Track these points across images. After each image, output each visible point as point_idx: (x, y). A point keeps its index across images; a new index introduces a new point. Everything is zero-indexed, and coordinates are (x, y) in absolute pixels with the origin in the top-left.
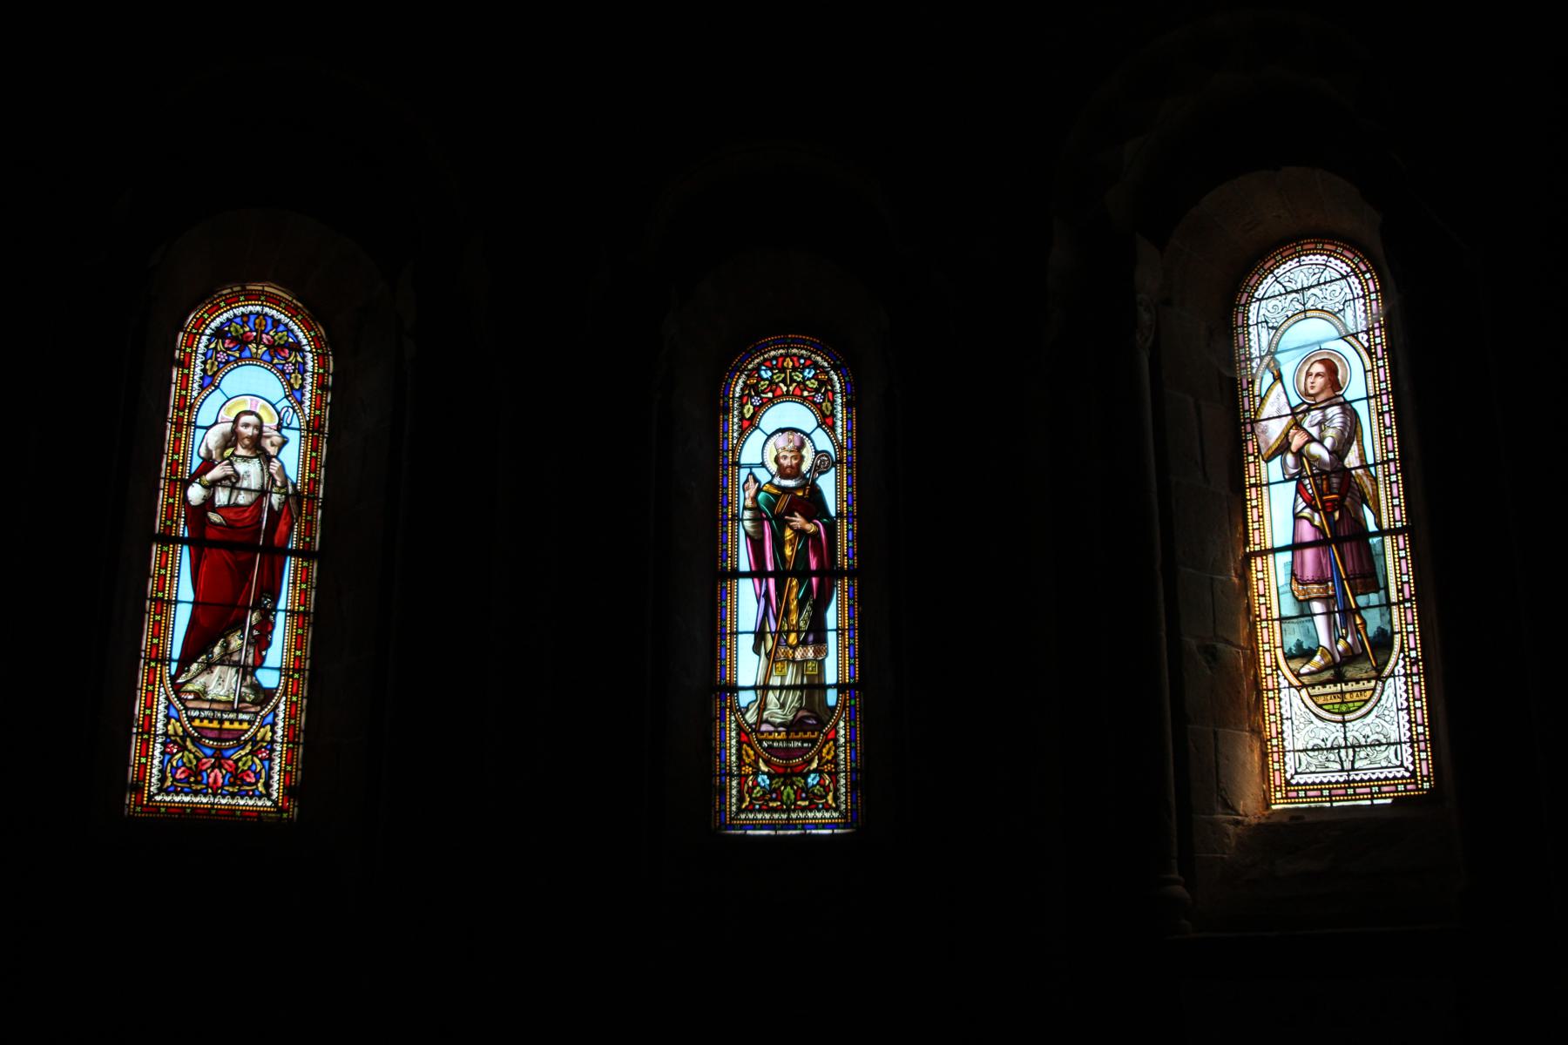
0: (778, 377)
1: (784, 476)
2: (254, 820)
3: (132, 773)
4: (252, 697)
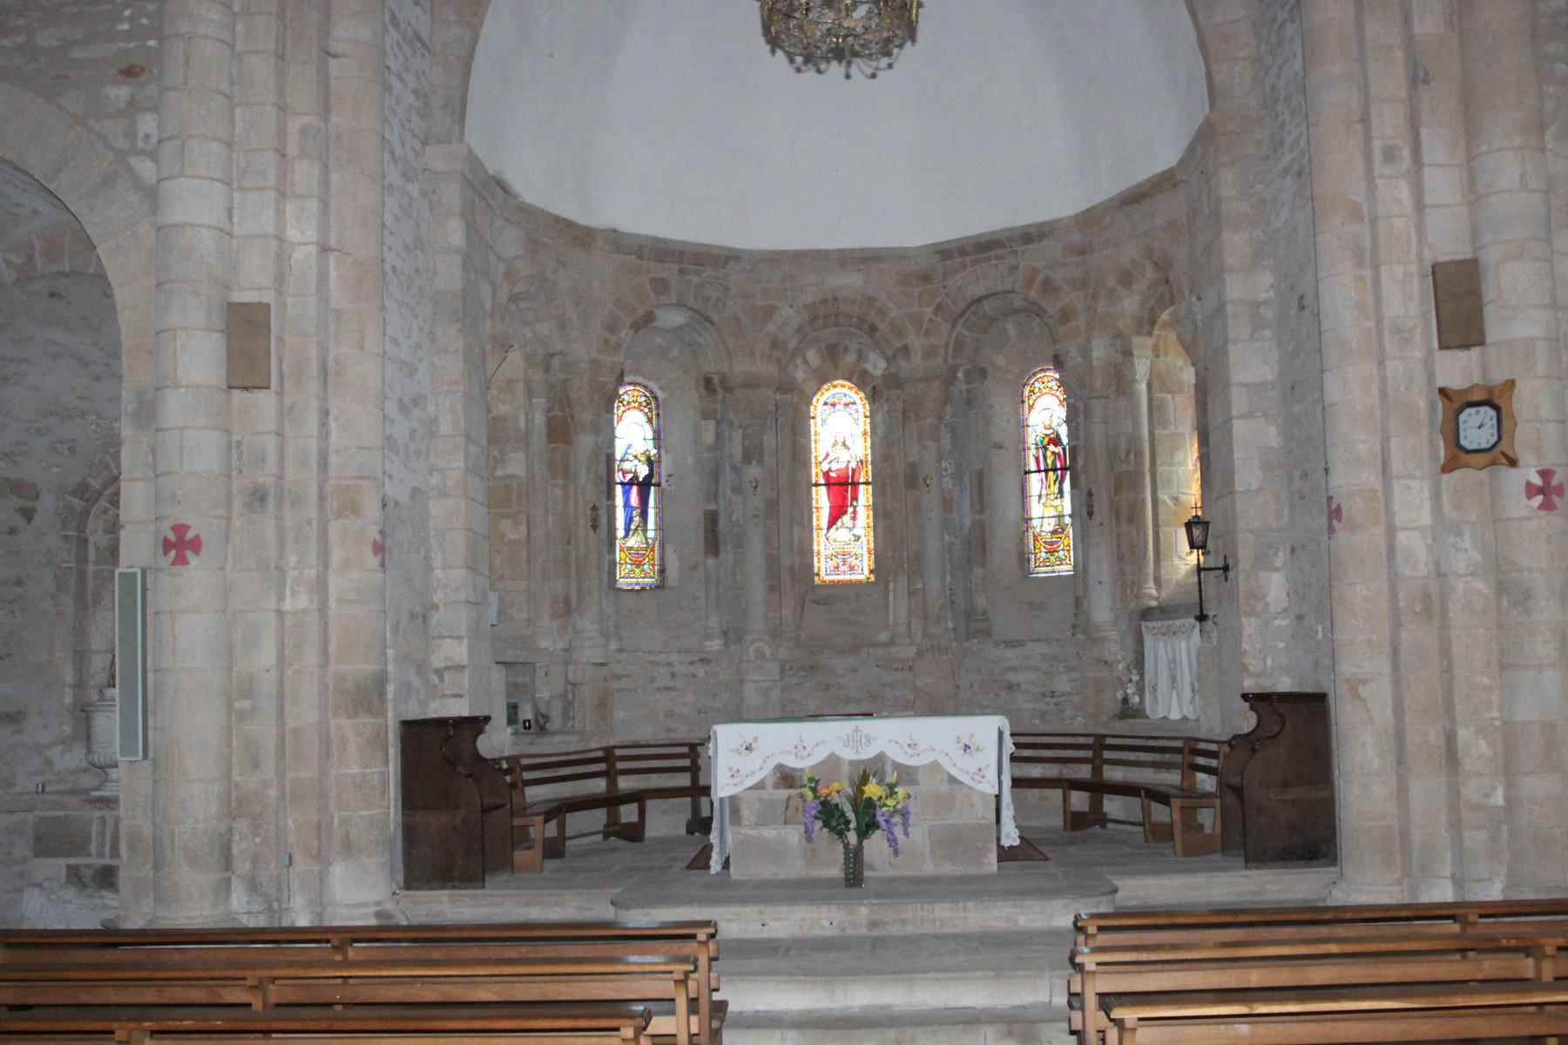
0: (1042, 386)
1: (1046, 429)
2: (859, 583)
3: (816, 570)
4: (1261, 311)
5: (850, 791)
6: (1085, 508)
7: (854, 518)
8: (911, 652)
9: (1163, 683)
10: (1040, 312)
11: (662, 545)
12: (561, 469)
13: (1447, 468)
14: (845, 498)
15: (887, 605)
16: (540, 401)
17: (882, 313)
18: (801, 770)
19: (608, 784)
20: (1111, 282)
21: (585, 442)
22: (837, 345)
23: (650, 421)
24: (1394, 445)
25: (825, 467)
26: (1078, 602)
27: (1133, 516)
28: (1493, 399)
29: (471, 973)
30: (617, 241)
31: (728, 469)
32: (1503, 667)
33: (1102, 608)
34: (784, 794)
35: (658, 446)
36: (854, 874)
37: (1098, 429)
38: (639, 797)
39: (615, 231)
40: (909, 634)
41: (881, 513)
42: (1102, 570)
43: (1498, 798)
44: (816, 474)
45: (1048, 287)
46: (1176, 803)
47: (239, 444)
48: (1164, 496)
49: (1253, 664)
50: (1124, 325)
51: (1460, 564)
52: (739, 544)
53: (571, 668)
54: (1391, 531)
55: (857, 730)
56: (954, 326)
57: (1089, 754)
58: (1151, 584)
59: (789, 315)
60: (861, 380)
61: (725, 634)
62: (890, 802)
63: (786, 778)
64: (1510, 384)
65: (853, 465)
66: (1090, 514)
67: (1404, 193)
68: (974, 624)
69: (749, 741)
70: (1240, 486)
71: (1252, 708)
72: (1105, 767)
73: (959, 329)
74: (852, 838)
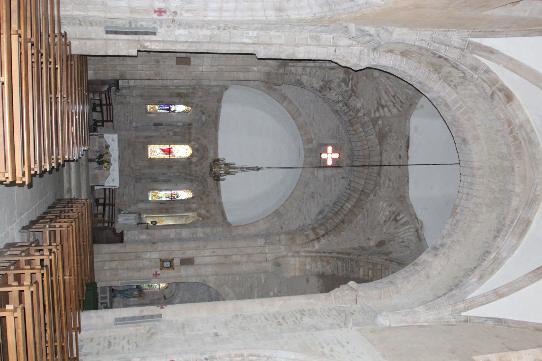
5: (105, 160)
6: (162, 203)
7: (162, 154)
8: (132, 166)
9: (126, 218)
10: (203, 194)
11: (156, 113)
12: (171, 95)
13: (161, 260)
14: (167, 152)
15: (142, 161)
16: (185, 91)
17: (205, 161)
18: (109, 150)
19: (104, 106)
20: (207, 208)
21: (177, 100)
22: (199, 151)
23: (183, 111)
24: (165, 252)
25: (173, 148)
26: (143, 201)
27: (160, 212)
28: (172, 267)
29: (32, 13)
30: (219, 108)
31: (172, 128)
32: (127, 268)
33: (141, 206)
34: (104, 146)
35: (178, 112)
36: (90, 160)
37: (178, 205)
38: (102, 111)
39: (221, 107)
40: (136, 166)
41: (163, 160)
42: (149, 206)
43: (106, 268)
44: (172, 146)
45: (208, 196)
46: (103, 218)
47: (167, 58)
48: (164, 218)
49: (129, 233)
50: (199, 211)
51: (144, 262)
52: (156, 130)
53: (129, 97)
54: (151, 252)
55: (116, 160)
56: (202, 176)
57: (111, 203)
58: (146, 216)
59: (205, 142)
60: (192, 156)
61: (136, 127)
62: (103, 167)
63: (107, 147)
64: (173, 269)
65: (174, 154)
66: (161, 204)
67: (207, 254)
68: (138, 179)
69: (115, 140)
70: (162, 230)
71: (121, 232)
72: (108, 206)
73: (201, 177)
74: (97, 160)
